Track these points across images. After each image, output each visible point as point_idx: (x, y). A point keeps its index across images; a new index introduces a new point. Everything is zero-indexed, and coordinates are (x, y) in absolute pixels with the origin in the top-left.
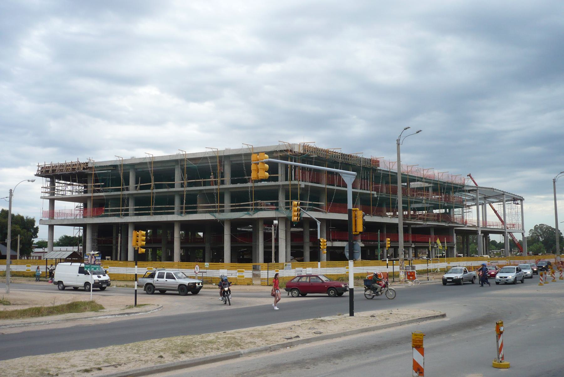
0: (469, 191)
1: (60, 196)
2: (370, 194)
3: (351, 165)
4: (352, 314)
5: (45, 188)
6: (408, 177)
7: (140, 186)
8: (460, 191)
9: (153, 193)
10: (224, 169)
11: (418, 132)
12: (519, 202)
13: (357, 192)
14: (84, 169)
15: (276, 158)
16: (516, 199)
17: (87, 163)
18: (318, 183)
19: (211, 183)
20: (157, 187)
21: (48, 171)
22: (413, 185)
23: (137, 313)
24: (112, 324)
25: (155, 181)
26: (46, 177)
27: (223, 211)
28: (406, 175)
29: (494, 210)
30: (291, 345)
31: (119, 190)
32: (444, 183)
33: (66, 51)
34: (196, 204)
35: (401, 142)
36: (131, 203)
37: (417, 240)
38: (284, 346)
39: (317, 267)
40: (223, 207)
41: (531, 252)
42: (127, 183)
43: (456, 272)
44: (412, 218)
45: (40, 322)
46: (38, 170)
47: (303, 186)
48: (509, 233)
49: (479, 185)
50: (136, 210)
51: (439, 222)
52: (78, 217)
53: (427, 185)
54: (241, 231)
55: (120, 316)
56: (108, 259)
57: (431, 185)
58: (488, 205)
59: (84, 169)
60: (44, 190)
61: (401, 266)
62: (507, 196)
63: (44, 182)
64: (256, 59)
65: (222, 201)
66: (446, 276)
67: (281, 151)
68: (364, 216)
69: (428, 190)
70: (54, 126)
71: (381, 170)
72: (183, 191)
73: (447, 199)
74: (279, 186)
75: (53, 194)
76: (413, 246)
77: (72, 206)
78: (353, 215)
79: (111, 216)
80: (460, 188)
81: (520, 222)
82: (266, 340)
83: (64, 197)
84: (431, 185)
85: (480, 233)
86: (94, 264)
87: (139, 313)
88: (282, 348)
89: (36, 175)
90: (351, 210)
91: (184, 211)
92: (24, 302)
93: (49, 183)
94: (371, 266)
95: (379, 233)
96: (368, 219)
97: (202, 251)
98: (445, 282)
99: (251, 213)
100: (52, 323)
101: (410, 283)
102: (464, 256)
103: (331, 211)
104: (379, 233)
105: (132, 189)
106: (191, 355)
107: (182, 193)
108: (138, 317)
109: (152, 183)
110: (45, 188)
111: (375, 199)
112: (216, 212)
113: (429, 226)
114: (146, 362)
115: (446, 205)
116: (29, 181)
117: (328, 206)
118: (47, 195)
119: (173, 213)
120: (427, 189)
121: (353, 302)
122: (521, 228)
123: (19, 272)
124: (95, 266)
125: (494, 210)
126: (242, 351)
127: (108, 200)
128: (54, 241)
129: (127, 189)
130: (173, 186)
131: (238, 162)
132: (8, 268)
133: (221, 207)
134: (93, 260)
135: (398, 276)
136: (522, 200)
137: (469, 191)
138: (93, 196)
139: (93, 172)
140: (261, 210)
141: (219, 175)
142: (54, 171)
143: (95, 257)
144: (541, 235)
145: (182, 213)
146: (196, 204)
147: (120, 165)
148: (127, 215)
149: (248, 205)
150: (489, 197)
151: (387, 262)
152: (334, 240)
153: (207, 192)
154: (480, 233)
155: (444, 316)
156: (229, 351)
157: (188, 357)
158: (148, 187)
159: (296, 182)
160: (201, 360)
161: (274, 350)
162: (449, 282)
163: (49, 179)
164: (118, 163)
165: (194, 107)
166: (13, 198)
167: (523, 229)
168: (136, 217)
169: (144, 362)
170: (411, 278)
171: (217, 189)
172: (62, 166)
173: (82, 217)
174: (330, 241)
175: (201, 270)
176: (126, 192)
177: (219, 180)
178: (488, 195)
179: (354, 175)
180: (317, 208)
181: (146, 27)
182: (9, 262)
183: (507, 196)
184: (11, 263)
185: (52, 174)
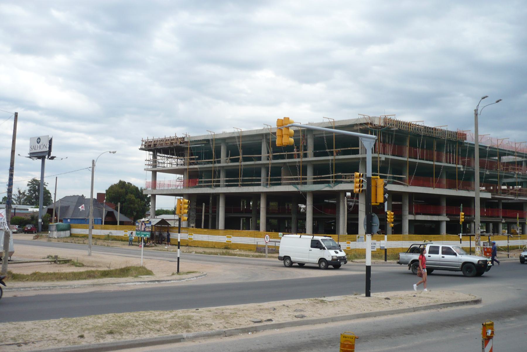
1: (161, 169)
2: (455, 168)
3: (435, 138)
4: (368, 295)
5: (149, 161)
6: (498, 151)
7: (230, 159)
9: (241, 165)
10: (306, 143)
11: (498, 102)
13: (441, 166)
14: (181, 143)
15: (356, 131)
17: (183, 138)
18: (402, 157)
19: (294, 156)
20: (245, 159)
21: (150, 145)
22: (505, 159)
23: (168, 281)
24: (132, 291)
25: (243, 154)
26: (149, 150)
27: (305, 183)
30: (255, 330)
31: (211, 162)
33: (192, 40)
34: (280, 176)
35: (479, 112)
36: (222, 175)
38: (245, 331)
39: (384, 239)
40: (306, 179)
42: (218, 155)
44: (503, 193)
45: (66, 286)
46: (142, 145)
47: (383, 159)
50: (227, 181)
52: (179, 188)
53: (519, 159)
54: (329, 203)
55: (150, 283)
56: (193, 227)
57: (524, 159)
59: (181, 143)
60: (147, 163)
61: (476, 242)
63: (148, 155)
64: (364, 41)
65: (305, 173)
67: (361, 124)
68: (385, 185)
69: (522, 165)
70: (182, 108)
71: (467, 143)
72: (268, 164)
74: (359, 159)
75: (155, 166)
76: (504, 221)
77: (173, 177)
78: (373, 184)
79: (205, 186)
82: (227, 323)
83: (164, 169)
84: (524, 159)
86: (144, 231)
87: (171, 280)
88: (240, 333)
89: (140, 149)
90: (370, 178)
91: (269, 182)
92: (99, 264)
93: (151, 156)
94: (452, 240)
95: (461, 207)
96: (392, 187)
97: (270, 220)
99: (331, 185)
100: (78, 288)
104: (461, 207)
105: (224, 162)
106: (119, 337)
107: (267, 166)
108: (168, 285)
109: (241, 157)
110: (149, 161)
111: (461, 173)
112: (298, 184)
113: (521, 201)
114: (60, 341)
116: (110, 152)
117: (410, 179)
118: (150, 167)
119: (259, 185)
120: (520, 163)
121: (370, 281)
123: (118, 236)
124: (145, 233)
126: (185, 334)
127: (202, 172)
128: (156, 209)
129: (219, 162)
130: (260, 159)
131: (319, 136)
132: (90, 231)
133: (303, 179)
134: (143, 227)
138: (189, 169)
139: (189, 146)
140: (341, 182)
141: (302, 148)
142: (155, 145)
143: (145, 224)
145: (267, 184)
146: (280, 176)
147: (212, 140)
148: (219, 186)
149: (329, 178)
151: (461, 237)
152: (417, 214)
153: (290, 165)
155: (477, 302)
156: (170, 334)
157: (114, 338)
158: (237, 160)
160: (127, 344)
161: (231, 335)
163: (151, 153)
164: (210, 138)
165: (307, 88)
166: (95, 168)
168: (226, 188)
171: (299, 162)
172: (162, 140)
173: (182, 188)
174: (413, 214)
175: (271, 240)
176: (217, 165)
177: (301, 153)
180: (400, 181)
181: (263, 15)
182: (91, 227)
184: (93, 228)
185: (155, 148)
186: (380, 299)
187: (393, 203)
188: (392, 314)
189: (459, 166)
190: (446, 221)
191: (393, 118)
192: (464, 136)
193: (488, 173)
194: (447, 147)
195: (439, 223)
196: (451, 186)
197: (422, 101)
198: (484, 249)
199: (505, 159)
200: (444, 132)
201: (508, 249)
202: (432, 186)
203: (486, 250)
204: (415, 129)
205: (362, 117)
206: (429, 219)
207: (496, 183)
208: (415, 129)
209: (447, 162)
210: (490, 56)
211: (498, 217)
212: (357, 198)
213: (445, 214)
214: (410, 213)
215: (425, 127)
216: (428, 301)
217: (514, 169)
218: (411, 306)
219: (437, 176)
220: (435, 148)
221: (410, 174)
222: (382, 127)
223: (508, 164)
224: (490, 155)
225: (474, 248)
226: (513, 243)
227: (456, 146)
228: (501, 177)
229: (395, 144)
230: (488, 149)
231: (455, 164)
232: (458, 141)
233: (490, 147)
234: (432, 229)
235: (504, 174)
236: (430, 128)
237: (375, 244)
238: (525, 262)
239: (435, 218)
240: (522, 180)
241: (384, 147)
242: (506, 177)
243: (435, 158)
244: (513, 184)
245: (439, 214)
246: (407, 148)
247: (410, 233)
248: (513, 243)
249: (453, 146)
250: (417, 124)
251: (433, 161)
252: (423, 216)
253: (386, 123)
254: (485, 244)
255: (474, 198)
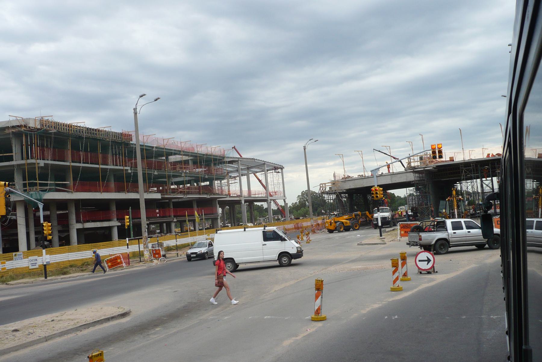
0: (231, 162)
2: (123, 170)
3: (100, 140)
6: (165, 150)
8: (221, 163)
12: (280, 170)
16: (277, 168)
18: (64, 161)
22: (172, 158)
28: (163, 149)
29: (259, 179)
32: (204, 155)
35: (138, 110)
37: (179, 214)
39: (42, 255)
41: (293, 217)
43: (200, 245)
47: (42, 165)
48: (274, 200)
49: (244, 156)
51: (200, 194)
53: (185, 158)
58: (252, 176)
61: (144, 245)
62: (268, 166)
64: (25, 38)
66: (190, 251)
67: (13, 127)
69: (188, 163)
71: (133, 144)
73: (209, 172)
74: (13, 166)
76: (175, 220)
80: (219, 160)
81: (282, 189)
85: (243, 202)
95: (130, 210)
98: (189, 258)
101: (155, 261)
102: (231, 226)
103: (77, 191)
104: (130, 210)
111: (128, 176)
113: (191, 199)
115: (207, 177)
117: (74, 185)
120: (186, 162)
122: (282, 195)
125: (259, 179)
135: (143, 255)
136: (282, 168)
137: (231, 162)
144: (307, 200)
150: (252, 167)
154: (243, 202)
155: (124, 315)
159: (33, 161)
162: (194, 257)
167: (284, 196)
169: (220, 272)
170: (157, 256)
178: (250, 165)
179: (493, 189)
180: (64, 188)
183: (268, 166)
186: (6, 333)
187: (58, 212)
188: (16, 350)
189: (126, 168)
190: (118, 226)
191: (50, 119)
192: (193, 148)
193: (156, 173)
194: (112, 149)
195: (110, 228)
196: (120, 189)
197: (94, 103)
198: (153, 250)
199: (172, 158)
200: (107, 133)
201: (178, 248)
202: (99, 191)
203: (154, 252)
204: (77, 131)
205: (14, 118)
206: (99, 226)
207: (165, 183)
208: (77, 131)
209: (113, 165)
210: (160, 59)
211: (170, 216)
212: (15, 209)
213: (116, 219)
214: (78, 221)
215: (88, 129)
216: (66, 324)
217: (181, 168)
218: (43, 335)
219: (103, 180)
220: (100, 151)
221: (75, 179)
222: (38, 129)
223: (175, 163)
224: (154, 155)
225: (142, 252)
226: (181, 241)
227: (122, 148)
228: (169, 177)
229: (54, 148)
230: (154, 149)
231: (122, 166)
232: (124, 142)
233: (156, 147)
234: (102, 236)
235: (172, 174)
236: (93, 129)
237: (36, 260)
238: (192, 259)
239: (105, 224)
240: (190, 178)
241: (43, 151)
242: (175, 176)
243: (100, 161)
244: (182, 183)
245: (109, 220)
246: (69, 153)
247: (79, 242)
248: (181, 241)
249: (119, 148)
250: (79, 125)
251: (98, 164)
252: (93, 223)
253: (43, 125)
254: (154, 246)
255: (139, 199)
